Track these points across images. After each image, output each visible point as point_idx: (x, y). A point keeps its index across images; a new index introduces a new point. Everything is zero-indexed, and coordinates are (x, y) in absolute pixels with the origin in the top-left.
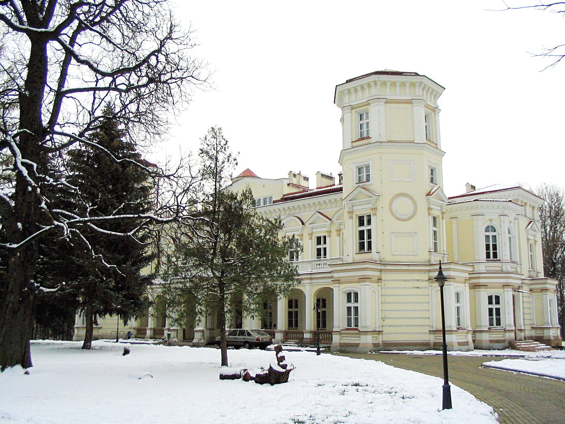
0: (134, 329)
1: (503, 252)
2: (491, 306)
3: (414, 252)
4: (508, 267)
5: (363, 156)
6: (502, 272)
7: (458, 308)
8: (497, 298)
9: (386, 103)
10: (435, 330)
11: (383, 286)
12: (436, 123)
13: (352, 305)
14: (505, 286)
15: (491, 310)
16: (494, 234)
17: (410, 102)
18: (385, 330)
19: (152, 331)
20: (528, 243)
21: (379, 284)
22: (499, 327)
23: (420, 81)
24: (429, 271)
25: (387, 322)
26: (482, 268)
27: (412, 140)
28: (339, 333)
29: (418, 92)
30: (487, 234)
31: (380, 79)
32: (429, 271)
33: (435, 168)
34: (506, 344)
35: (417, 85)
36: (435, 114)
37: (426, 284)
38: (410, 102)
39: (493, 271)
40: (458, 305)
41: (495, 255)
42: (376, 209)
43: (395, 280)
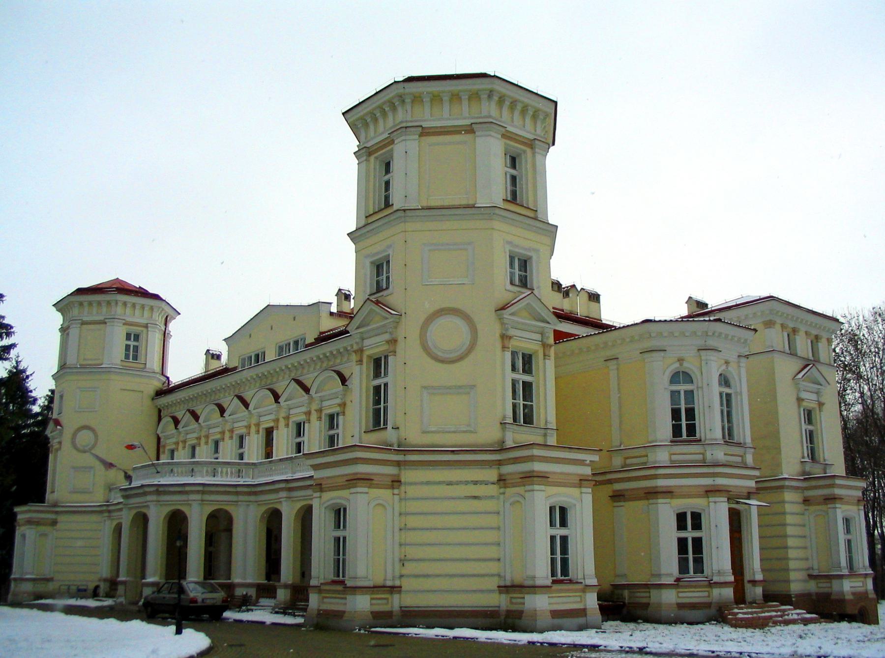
0: (105, 580)
1: (710, 424)
2: (683, 534)
3: (469, 425)
4: (719, 454)
5: (385, 240)
6: (704, 464)
7: (849, 541)
8: (697, 518)
9: (421, 135)
10: (508, 583)
11: (403, 495)
12: (539, 174)
13: (690, 534)
14: (710, 492)
15: (682, 543)
16: (689, 387)
17: (470, 130)
18: (406, 584)
19: (108, 584)
20: (799, 406)
21: (396, 491)
22: (699, 578)
23: (489, 87)
24: (500, 463)
25: (410, 568)
26: (662, 456)
27: (471, 202)
28: (319, 589)
29: (490, 109)
30: (675, 388)
31: (407, 91)
32: (500, 463)
33: (530, 258)
34: (713, 611)
35: (484, 96)
36: (534, 154)
37: (493, 490)
38: (470, 130)
39: (692, 462)
40: (849, 537)
41: (691, 430)
42: (394, 341)
43: (428, 483)
